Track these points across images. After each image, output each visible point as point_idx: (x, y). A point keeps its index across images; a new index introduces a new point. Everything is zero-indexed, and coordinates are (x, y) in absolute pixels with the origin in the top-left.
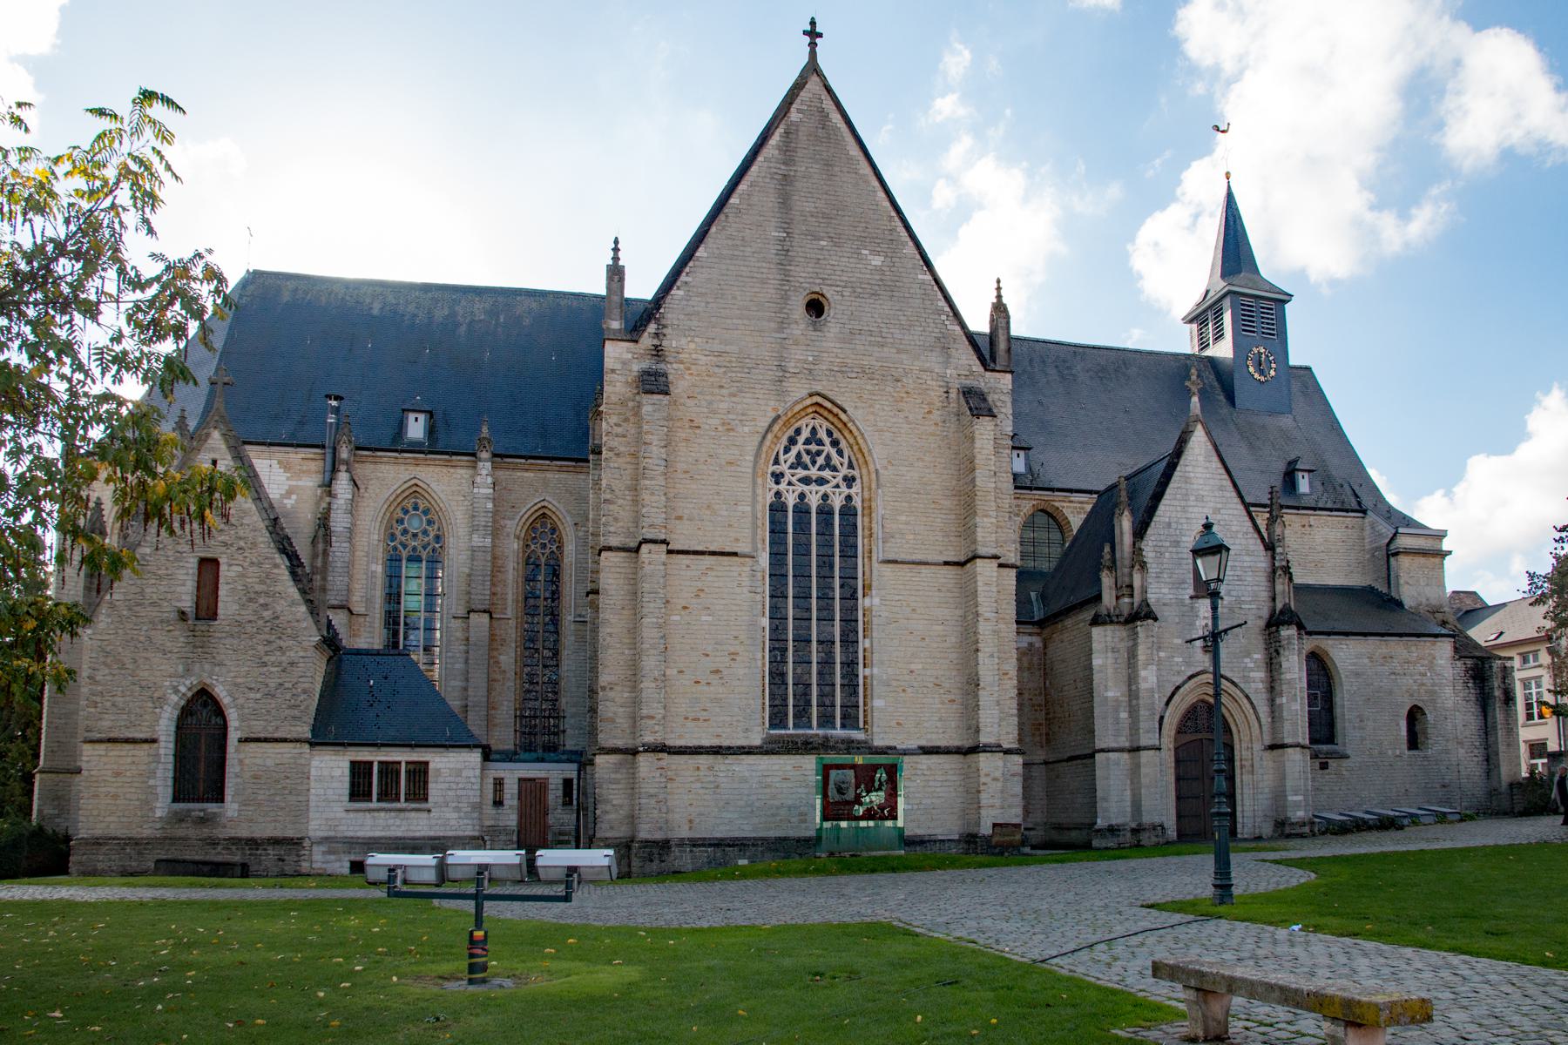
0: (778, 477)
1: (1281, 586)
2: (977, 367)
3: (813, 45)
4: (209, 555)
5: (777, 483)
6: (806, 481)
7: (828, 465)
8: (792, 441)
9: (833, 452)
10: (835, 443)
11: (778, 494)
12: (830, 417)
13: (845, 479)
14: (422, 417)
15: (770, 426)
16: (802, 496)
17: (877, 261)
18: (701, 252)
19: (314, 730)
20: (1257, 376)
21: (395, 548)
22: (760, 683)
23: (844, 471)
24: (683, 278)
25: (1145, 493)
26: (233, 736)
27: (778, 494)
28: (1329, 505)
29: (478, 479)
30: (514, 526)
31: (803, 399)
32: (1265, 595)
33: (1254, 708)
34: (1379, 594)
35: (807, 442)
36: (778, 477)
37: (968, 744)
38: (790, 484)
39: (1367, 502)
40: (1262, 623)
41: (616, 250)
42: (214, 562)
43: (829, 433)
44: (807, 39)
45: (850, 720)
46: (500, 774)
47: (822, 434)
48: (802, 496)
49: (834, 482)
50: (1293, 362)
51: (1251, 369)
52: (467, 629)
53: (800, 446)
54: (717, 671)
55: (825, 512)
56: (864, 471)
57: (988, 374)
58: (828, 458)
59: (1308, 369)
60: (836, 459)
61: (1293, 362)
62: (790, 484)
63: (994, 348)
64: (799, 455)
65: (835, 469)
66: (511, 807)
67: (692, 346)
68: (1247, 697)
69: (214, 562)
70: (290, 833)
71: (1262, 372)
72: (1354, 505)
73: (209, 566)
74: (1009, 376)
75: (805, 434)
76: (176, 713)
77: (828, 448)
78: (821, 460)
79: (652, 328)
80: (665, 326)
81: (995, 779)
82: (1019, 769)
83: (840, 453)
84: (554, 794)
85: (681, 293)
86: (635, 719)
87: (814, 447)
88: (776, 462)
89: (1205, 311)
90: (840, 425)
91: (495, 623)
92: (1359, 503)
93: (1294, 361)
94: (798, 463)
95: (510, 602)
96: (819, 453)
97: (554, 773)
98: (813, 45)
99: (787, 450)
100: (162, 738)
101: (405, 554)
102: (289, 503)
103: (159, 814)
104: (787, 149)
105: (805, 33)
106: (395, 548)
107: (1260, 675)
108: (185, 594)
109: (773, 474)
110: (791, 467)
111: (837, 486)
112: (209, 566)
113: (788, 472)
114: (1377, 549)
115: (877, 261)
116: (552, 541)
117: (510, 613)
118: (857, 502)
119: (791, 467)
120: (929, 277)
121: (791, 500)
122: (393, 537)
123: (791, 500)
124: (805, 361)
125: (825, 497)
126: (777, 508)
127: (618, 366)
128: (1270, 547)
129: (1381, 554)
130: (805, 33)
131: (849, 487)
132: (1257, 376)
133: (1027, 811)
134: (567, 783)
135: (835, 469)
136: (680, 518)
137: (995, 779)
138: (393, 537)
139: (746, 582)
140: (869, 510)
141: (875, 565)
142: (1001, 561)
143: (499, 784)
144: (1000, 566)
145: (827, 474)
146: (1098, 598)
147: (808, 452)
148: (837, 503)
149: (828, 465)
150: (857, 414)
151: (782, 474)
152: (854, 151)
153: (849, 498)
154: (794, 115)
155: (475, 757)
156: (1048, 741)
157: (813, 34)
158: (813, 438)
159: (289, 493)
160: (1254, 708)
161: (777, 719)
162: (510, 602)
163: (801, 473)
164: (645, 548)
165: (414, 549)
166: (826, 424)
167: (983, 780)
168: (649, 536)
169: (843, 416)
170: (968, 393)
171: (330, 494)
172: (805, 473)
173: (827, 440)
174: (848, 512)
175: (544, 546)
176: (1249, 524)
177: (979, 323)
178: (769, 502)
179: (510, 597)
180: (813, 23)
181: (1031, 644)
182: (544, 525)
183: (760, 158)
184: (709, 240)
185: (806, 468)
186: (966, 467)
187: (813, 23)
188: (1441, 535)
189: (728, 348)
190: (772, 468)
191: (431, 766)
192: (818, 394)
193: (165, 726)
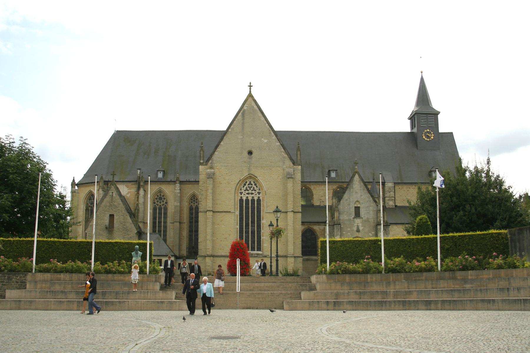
0: (241, 193)
3: (250, 89)
6: (248, 194)
7: (254, 190)
8: (245, 185)
9: (255, 187)
10: (255, 185)
11: (241, 197)
13: (258, 193)
14: (162, 173)
15: (238, 183)
16: (247, 197)
17: (266, 141)
20: (426, 139)
23: (258, 191)
27: (241, 197)
30: (186, 199)
35: (249, 185)
36: (241, 193)
42: (113, 215)
43: (254, 182)
45: (259, 249)
47: (252, 183)
48: (247, 197)
51: (424, 137)
53: (247, 186)
55: (253, 200)
64: (246, 188)
65: (255, 191)
69: (113, 215)
71: (428, 137)
73: (112, 216)
75: (248, 183)
77: (254, 186)
78: (252, 189)
79: (210, 161)
82: (302, 261)
83: (257, 187)
86: (213, 247)
87: (250, 186)
88: (241, 190)
93: (442, 129)
94: (246, 190)
98: (250, 89)
99: (243, 187)
101: (158, 207)
102: (128, 195)
104: (243, 115)
112: (112, 216)
113: (244, 192)
115: (266, 141)
116: (196, 202)
117: (185, 221)
118: (261, 198)
121: (244, 198)
122: (154, 203)
123: (244, 198)
125: (253, 197)
126: (241, 200)
132: (426, 139)
135: (255, 191)
138: (154, 203)
139: (233, 218)
145: (253, 192)
148: (256, 198)
149: (254, 190)
152: (260, 115)
153: (259, 197)
154: (245, 108)
158: (250, 184)
159: (128, 193)
173: (253, 184)
174: (259, 200)
180: (250, 83)
187: (250, 83)
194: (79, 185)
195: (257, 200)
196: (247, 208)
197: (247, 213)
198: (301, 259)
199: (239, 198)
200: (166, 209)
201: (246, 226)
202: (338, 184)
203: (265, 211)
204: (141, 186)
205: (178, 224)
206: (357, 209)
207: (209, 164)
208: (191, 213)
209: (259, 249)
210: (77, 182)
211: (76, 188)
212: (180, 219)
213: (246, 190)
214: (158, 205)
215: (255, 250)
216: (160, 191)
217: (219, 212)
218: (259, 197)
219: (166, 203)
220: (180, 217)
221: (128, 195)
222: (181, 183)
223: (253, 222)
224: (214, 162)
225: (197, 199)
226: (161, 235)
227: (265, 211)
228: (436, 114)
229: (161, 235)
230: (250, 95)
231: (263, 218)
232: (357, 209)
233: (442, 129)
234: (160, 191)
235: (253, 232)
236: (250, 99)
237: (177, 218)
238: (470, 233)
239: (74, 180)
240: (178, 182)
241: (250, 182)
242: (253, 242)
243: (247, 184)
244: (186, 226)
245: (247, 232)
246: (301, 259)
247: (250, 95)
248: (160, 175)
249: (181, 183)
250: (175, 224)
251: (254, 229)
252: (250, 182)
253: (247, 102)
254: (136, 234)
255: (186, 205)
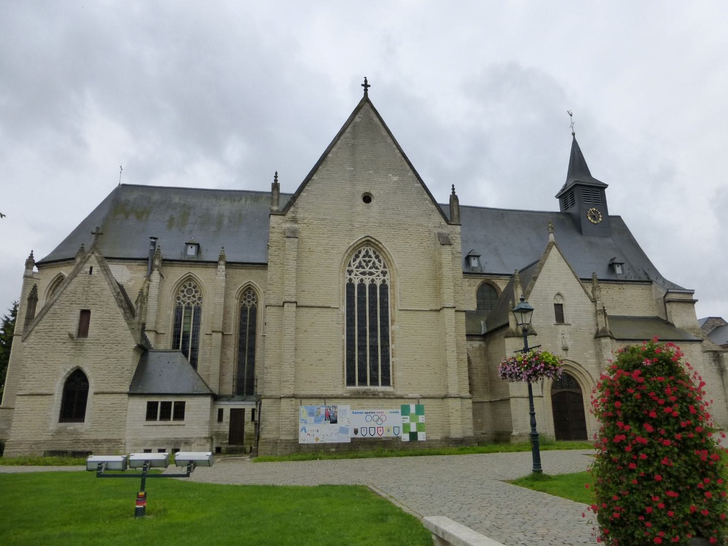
0: (350, 272)
1: (601, 319)
2: (444, 223)
3: (366, 90)
4: (86, 308)
5: (350, 275)
6: (363, 273)
7: (374, 266)
8: (357, 256)
9: (376, 261)
10: (377, 257)
11: (350, 280)
12: (375, 246)
13: (382, 272)
16: (362, 280)
18: (315, 177)
19: (131, 387)
20: (592, 221)
21: (179, 303)
22: (341, 365)
23: (381, 269)
24: (307, 188)
25: (528, 276)
26: (91, 391)
27: (350, 280)
28: (633, 279)
29: (219, 273)
30: (235, 293)
31: (362, 239)
32: (593, 323)
33: (591, 376)
34: (663, 320)
35: (364, 256)
36: (350, 272)
37: (443, 394)
38: (356, 275)
39: (652, 278)
40: (593, 336)
41: (276, 177)
43: (374, 253)
44: (363, 88)
45: (386, 382)
46: (221, 407)
47: (371, 253)
48: (362, 280)
49: (377, 274)
50: (610, 213)
51: (589, 218)
52: (211, 340)
53: (361, 258)
54: (321, 360)
55: (373, 287)
56: (391, 269)
57: (449, 226)
58: (374, 263)
59: (619, 217)
60: (377, 264)
61: (610, 213)
62: (356, 275)
63: (453, 212)
64: (360, 262)
65: (377, 268)
66: (226, 422)
67: (310, 216)
68: (587, 372)
70: (115, 437)
72: (645, 279)
74: (459, 227)
75: (363, 253)
76: (64, 381)
77: (374, 259)
78: (370, 264)
79: (292, 209)
80: (297, 208)
81: (457, 410)
82: (471, 405)
83: (380, 261)
84: (248, 416)
85: (305, 194)
87: (367, 259)
88: (350, 265)
89: (566, 193)
90: (379, 249)
91: (225, 337)
92: (648, 278)
93: (611, 212)
94: (360, 266)
95: (232, 327)
96: (370, 261)
97: (248, 407)
98: (366, 90)
99: (354, 260)
100: (56, 392)
101: (184, 306)
102: (131, 284)
103: (51, 428)
105: (362, 85)
106: (179, 303)
107: (593, 360)
108: (73, 326)
109: (348, 271)
110: (357, 268)
111: (378, 276)
114: (659, 299)
115: (395, 179)
116: (253, 300)
118: (388, 283)
119: (357, 268)
120: (420, 185)
121: (356, 282)
123: (356, 282)
124: (362, 222)
125: (373, 280)
126: (350, 286)
127: (275, 226)
128: (594, 301)
129: (661, 302)
130: (362, 85)
131: (384, 276)
132: (592, 221)
133: (477, 425)
134: (253, 410)
135: (377, 268)
136: (303, 291)
137: (457, 410)
138: (179, 298)
140: (393, 286)
141: (397, 311)
142: (456, 309)
143: (221, 412)
144: (456, 311)
145: (373, 270)
146: (507, 325)
147: (364, 261)
148: (378, 283)
150: (387, 245)
151: (352, 271)
152: (385, 133)
153: (384, 281)
155: (208, 400)
156: (491, 391)
157: (366, 86)
158: (367, 255)
159: (131, 280)
160: (591, 376)
161: (351, 382)
162: (232, 327)
163: (361, 270)
164: (286, 305)
165: (189, 304)
166: (372, 249)
167: (451, 411)
168: (288, 300)
169: (380, 245)
170: (440, 235)
171: (150, 280)
172: (363, 270)
173: (373, 256)
174: (384, 287)
175: (249, 302)
176: (582, 290)
177: (443, 198)
178: (346, 283)
179: (233, 325)
180: (366, 81)
181: (480, 345)
182: (249, 293)
183: (342, 138)
184: (318, 172)
185: (363, 268)
186: (437, 267)
187: (366, 81)
188: (691, 293)
189: (326, 217)
190: (347, 268)
191: (186, 404)
192: (368, 236)
193: (58, 390)
194: (41, 265)
195: (381, 285)
196: (362, 302)
197: (362, 311)
198: (470, 401)
199: (347, 281)
200: (198, 310)
201: (359, 336)
202: (484, 277)
203: (399, 306)
204: (156, 266)
205: (220, 335)
206: (559, 308)
207: (290, 215)
208: (243, 318)
209: (386, 382)
210: (37, 259)
211: (35, 269)
212: (224, 328)
213: (360, 266)
214: (184, 302)
215: (377, 384)
216: (190, 278)
217: (303, 307)
218: (384, 281)
219: (200, 299)
220: (224, 323)
221: (131, 284)
222: (229, 265)
223: (373, 329)
224: (299, 210)
225: (254, 295)
226: (186, 356)
227: (399, 306)
228: (601, 188)
229: (186, 356)
230: (366, 100)
231: (393, 321)
232: (559, 308)
233: (611, 212)
234: (190, 278)
235: (374, 348)
236: (367, 106)
237: (218, 325)
238: (246, 371)
239: (31, 256)
240: (222, 262)
241: (367, 252)
242: (374, 368)
243: (361, 255)
244: (233, 341)
245: (362, 348)
246: (470, 401)
247: (366, 100)
248: (191, 251)
249: (229, 265)
250: (214, 334)
251: (376, 342)
252: (367, 252)
253: (362, 111)
254: (135, 349)
255: (234, 304)
